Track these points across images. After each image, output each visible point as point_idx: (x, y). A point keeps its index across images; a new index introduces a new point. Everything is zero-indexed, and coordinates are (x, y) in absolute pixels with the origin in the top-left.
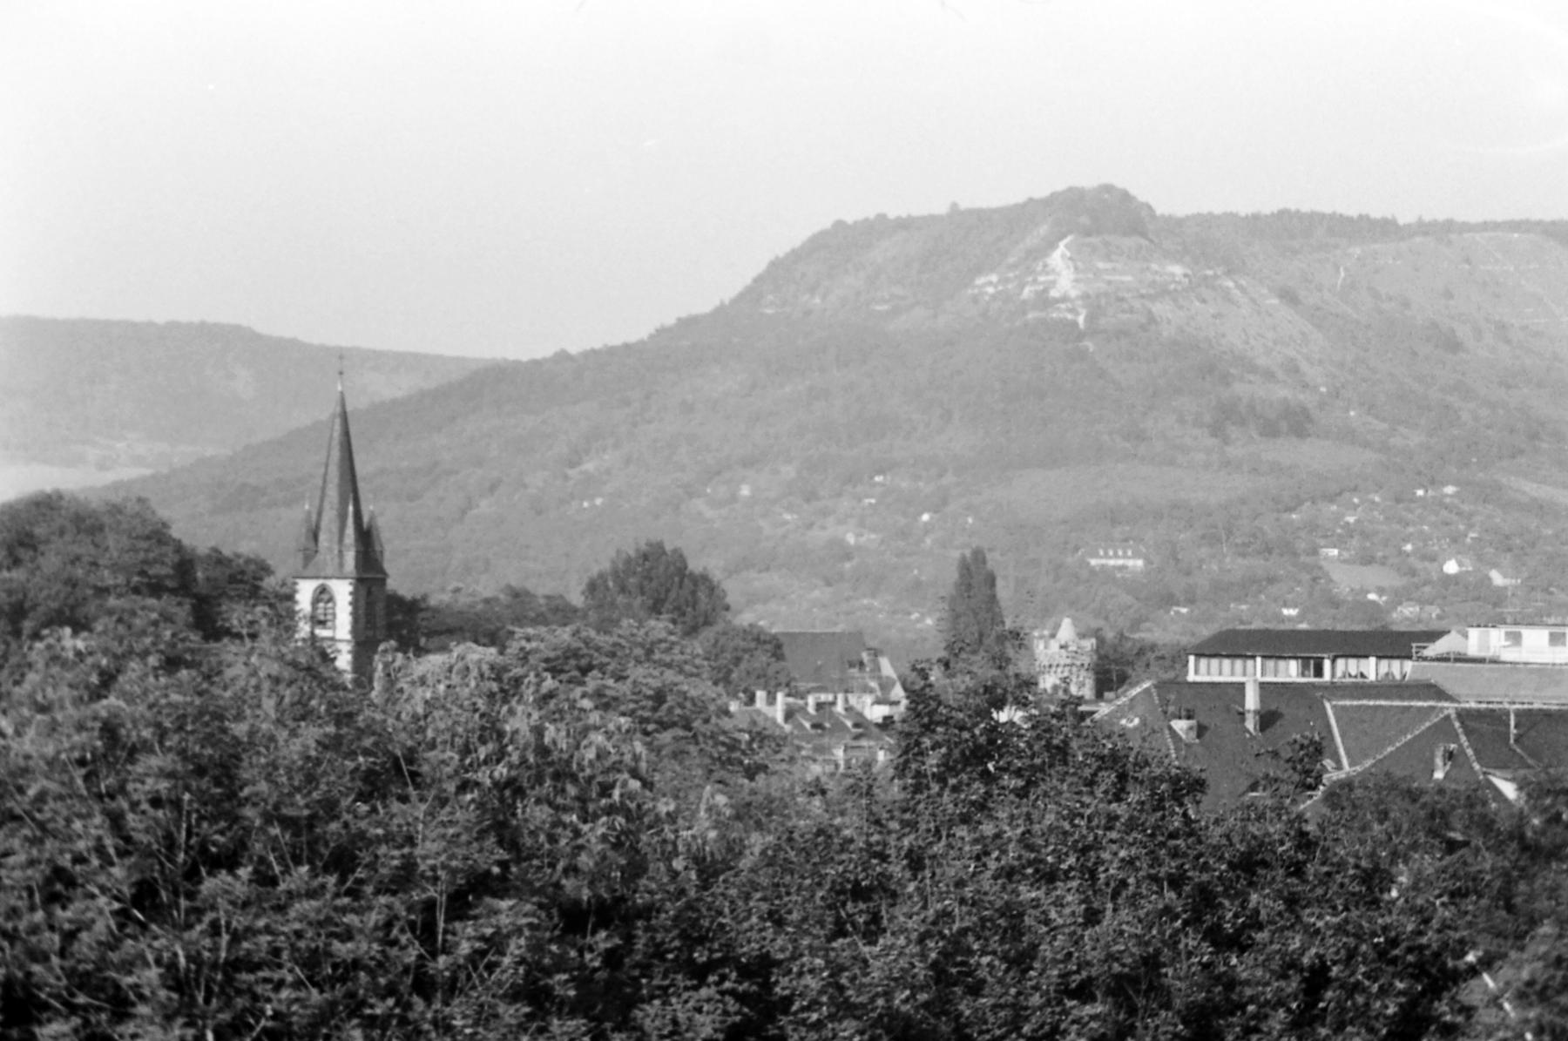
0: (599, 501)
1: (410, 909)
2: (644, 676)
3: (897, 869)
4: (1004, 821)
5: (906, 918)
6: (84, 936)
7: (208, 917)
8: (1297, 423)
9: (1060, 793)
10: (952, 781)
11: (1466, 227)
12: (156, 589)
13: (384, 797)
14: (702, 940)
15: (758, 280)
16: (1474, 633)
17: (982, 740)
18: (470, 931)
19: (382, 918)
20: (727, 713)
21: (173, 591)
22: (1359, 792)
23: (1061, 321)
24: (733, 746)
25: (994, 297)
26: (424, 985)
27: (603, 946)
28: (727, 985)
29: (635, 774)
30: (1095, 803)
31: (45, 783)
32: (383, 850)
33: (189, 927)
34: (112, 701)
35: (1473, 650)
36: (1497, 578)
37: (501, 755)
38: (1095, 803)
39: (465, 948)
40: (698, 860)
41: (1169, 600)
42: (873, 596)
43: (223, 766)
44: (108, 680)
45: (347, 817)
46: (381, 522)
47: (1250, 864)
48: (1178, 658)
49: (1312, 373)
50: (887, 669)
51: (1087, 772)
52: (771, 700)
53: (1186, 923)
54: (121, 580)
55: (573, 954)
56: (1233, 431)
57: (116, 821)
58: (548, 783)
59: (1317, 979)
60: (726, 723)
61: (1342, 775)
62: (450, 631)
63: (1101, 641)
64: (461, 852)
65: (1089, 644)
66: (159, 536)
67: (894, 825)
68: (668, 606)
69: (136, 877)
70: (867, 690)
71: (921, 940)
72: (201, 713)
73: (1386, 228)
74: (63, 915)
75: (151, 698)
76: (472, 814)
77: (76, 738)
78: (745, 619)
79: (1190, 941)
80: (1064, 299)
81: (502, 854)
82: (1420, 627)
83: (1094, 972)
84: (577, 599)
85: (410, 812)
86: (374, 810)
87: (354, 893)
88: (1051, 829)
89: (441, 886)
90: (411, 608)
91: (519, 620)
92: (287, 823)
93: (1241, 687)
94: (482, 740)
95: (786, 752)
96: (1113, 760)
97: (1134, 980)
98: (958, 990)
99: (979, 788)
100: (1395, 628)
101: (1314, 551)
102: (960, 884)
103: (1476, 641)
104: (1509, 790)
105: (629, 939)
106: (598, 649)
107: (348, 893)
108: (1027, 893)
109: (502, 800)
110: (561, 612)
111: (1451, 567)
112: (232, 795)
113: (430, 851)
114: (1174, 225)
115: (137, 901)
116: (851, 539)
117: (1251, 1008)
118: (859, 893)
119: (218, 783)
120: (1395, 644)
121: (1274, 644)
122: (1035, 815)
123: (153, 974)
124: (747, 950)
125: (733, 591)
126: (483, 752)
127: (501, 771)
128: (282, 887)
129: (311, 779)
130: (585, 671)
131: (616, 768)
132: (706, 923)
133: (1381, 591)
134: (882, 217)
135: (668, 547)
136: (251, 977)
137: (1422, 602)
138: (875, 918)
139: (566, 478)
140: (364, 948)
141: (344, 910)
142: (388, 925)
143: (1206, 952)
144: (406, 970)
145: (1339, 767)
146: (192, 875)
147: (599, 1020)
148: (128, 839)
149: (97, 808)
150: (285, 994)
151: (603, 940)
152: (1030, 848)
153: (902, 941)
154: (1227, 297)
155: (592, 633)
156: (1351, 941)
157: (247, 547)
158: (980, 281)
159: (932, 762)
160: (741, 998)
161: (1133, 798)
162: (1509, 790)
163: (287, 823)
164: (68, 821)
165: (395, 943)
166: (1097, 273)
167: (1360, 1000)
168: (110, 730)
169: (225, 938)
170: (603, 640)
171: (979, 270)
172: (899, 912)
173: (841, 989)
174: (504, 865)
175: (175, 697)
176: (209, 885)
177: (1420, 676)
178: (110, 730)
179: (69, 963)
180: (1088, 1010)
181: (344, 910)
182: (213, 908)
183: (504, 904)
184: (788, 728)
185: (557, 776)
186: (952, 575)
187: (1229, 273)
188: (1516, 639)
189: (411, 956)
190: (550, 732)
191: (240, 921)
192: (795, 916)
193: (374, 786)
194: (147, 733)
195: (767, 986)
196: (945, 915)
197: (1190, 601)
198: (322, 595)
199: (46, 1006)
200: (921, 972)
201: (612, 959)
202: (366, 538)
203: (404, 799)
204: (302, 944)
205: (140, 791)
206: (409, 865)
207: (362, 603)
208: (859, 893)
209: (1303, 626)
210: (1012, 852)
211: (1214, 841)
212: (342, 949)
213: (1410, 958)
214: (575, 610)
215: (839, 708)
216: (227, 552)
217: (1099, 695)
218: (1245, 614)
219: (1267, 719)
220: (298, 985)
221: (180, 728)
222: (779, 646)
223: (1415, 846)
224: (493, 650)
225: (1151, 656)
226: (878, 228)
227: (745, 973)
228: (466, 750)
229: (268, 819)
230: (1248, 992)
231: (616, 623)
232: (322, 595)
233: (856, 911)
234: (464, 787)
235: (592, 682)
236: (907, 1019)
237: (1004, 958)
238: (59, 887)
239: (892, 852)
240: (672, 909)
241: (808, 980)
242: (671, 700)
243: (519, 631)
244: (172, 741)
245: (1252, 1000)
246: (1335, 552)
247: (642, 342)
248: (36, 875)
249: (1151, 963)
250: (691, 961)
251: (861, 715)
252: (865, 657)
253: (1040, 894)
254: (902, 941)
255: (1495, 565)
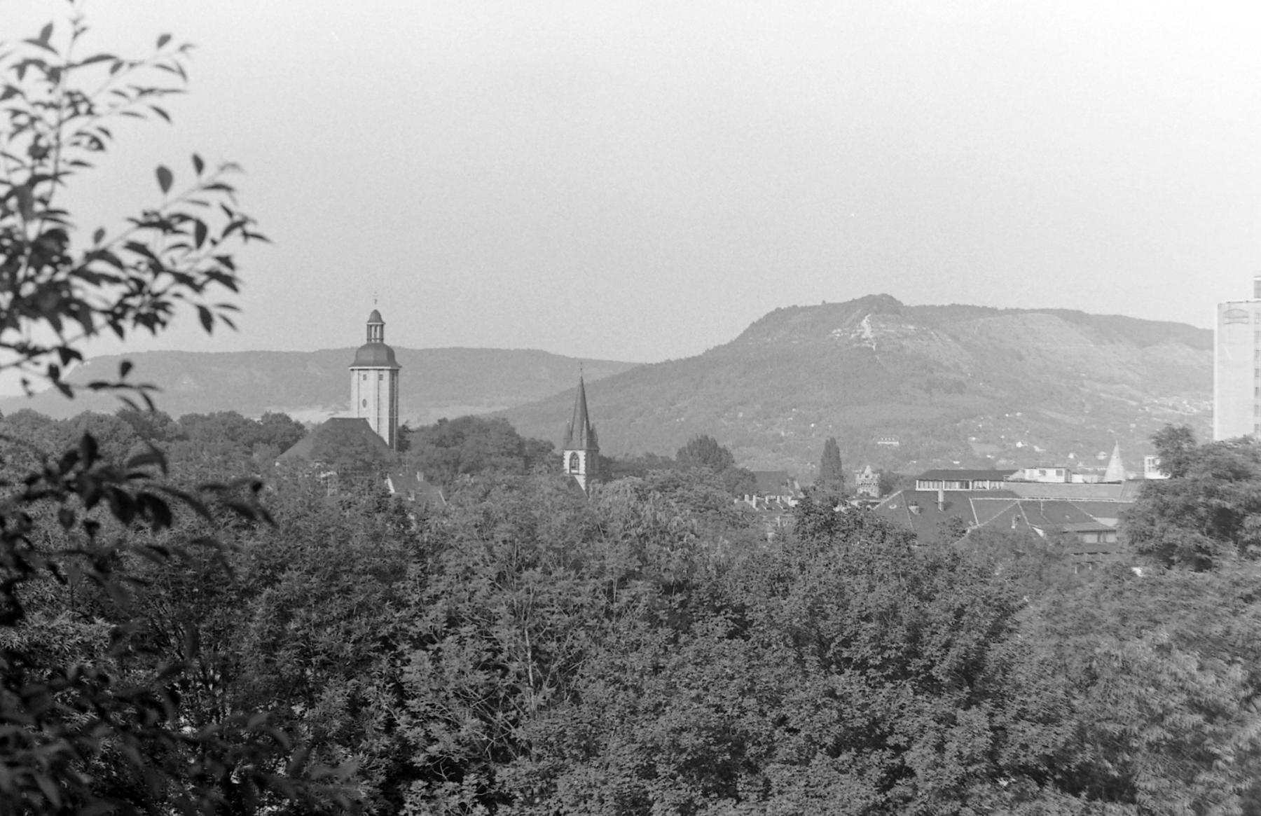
0: (683, 419)
1: (603, 584)
2: (700, 489)
3: (795, 570)
4: (837, 551)
5: (797, 590)
6: (477, 593)
7: (526, 586)
8: (960, 387)
9: (859, 544)
10: (817, 535)
11: (1023, 311)
12: (510, 454)
13: (592, 540)
14: (718, 598)
15: (746, 331)
16: (1028, 471)
17: (829, 519)
18: (626, 593)
19: (592, 589)
20: (733, 503)
21: (517, 455)
22: (982, 535)
23: (867, 348)
24: (735, 517)
25: (840, 338)
26: (609, 614)
27: (678, 600)
28: (728, 615)
29: (692, 532)
30: (874, 543)
31: (463, 535)
32: (592, 561)
33: (518, 590)
34: (488, 502)
35: (1027, 477)
36: (1037, 449)
37: (640, 523)
38: (874, 543)
39: (624, 600)
40: (717, 566)
41: (909, 458)
42: (792, 456)
43: (529, 527)
44: (486, 495)
45: (579, 548)
46: (597, 427)
47: (934, 568)
48: (912, 482)
49: (965, 368)
50: (797, 486)
51: (870, 532)
52: (751, 499)
53: (909, 591)
54: (496, 450)
55: (667, 602)
56: (934, 390)
57: (490, 549)
58: (658, 535)
59: (959, 613)
60: (733, 508)
61: (975, 527)
62: (624, 471)
63: (882, 474)
64: (623, 562)
65: (877, 476)
66: (511, 433)
67: (795, 552)
68: (710, 460)
69: (497, 571)
70: (789, 494)
71: (804, 598)
72: (521, 508)
73: (993, 311)
74: (470, 586)
75: (502, 502)
76: (628, 547)
77: (474, 517)
78: (740, 466)
79: (911, 598)
80: (867, 339)
81: (639, 563)
82: (1007, 469)
83: (872, 610)
84: (674, 458)
85: (604, 547)
86: (589, 546)
87: (581, 578)
88: (856, 554)
89: (615, 575)
90: (609, 461)
91: (651, 467)
92: (554, 550)
93: (937, 492)
94: (632, 518)
95: (756, 519)
96: (880, 526)
97: (887, 614)
98: (819, 618)
99: (827, 538)
100: (998, 469)
101: (966, 438)
102: (819, 576)
103: (1029, 474)
104: (1040, 532)
105: (690, 596)
106: (681, 478)
107: (580, 578)
108: (845, 579)
109: (640, 541)
110: (667, 463)
111: (1019, 445)
112: (534, 539)
113: (610, 562)
114: (910, 310)
115: (498, 579)
116: (783, 434)
117: (934, 625)
118: (780, 579)
119: (529, 535)
120: (997, 475)
121: (949, 476)
122: (850, 548)
123: (504, 608)
124: (736, 603)
125: (736, 454)
126: (632, 523)
127: (640, 530)
128: (553, 575)
129: (564, 533)
130: (676, 487)
131: (685, 529)
132: (720, 591)
133: (992, 454)
134: (795, 306)
135: (710, 437)
136: (542, 610)
137: (1007, 458)
138: (787, 590)
139: (670, 410)
140: (586, 599)
141: (577, 585)
142: (595, 590)
143: (916, 602)
144: (602, 609)
145: (975, 524)
146: (519, 569)
147: (677, 629)
148: (494, 556)
149: (482, 543)
150: (555, 617)
151: (679, 597)
152: (848, 562)
153: (796, 599)
154: (931, 338)
155: (679, 472)
156: (973, 597)
157: (545, 438)
158: (834, 331)
159: (810, 527)
160: (734, 620)
161: (888, 542)
162: (1040, 532)
163: (554, 550)
164: (471, 549)
165: (597, 597)
166: (880, 329)
167: (977, 620)
168: (487, 514)
169: (532, 595)
170: (684, 475)
171: (834, 327)
172: (796, 586)
173: (771, 617)
174: (640, 567)
175: (512, 501)
176: (526, 574)
177: (1008, 488)
178: (487, 514)
179: (472, 604)
180: (870, 625)
181: (577, 585)
182: (527, 583)
183: (639, 583)
184: (757, 509)
185: (661, 532)
186: (823, 448)
187: (932, 329)
188: (1044, 473)
189: (603, 602)
190: (659, 515)
191: (537, 588)
192: (753, 589)
193: (588, 537)
194: (501, 515)
195: (744, 616)
196: (814, 589)
197: (917, 459)
198: (574, 457)
199: (463, 620)
200: (804, 610)
201: (683, 604)
202: (591, 434)
203: (600, 541)
204: (561, 597)
205: (499, 537)
206: (602, 568)
207: (590, 463)
208: (780, 579)
209: (962, 468)
210: (840, 562)
211: (920, 558)
212: (577, 600)
213: (996, 603)
214: (673, 462)
215: (778, 501)
216: (537, 439)
217: (881, 496)
218: (938, 464)
219: (947, 506)
220: (560, 613)
221: (514, 514)
222: (754, 477)
223: (1005, 556)
224: (640, 479)
225: (901, 480)
226: (794, 310)
227: (735, 610)
228: (626, 522)
229: (548, 549)
230: (933, 618)
231: (689, 468)
232: (574, 457)
233: (779, 586)
234: (625, 537)
235: (679, 491)
236: (798, 628)
237: (837, 605)
238: (468, 574)
239: (793, 563)
240: (707, 585)
241: (760, 614)
242: (710, 498)
243: (651, 472)
244: (510, 518)
245: (934, 621)
246: (974, 439)
247: (700, 356)
248: (460, 570)
249: (894, 607)
250: (714, 606)
251: (786, 504)
252: (788, 481)
253: (851, 580)
254: (796, 599)
255: (1036, 444)
